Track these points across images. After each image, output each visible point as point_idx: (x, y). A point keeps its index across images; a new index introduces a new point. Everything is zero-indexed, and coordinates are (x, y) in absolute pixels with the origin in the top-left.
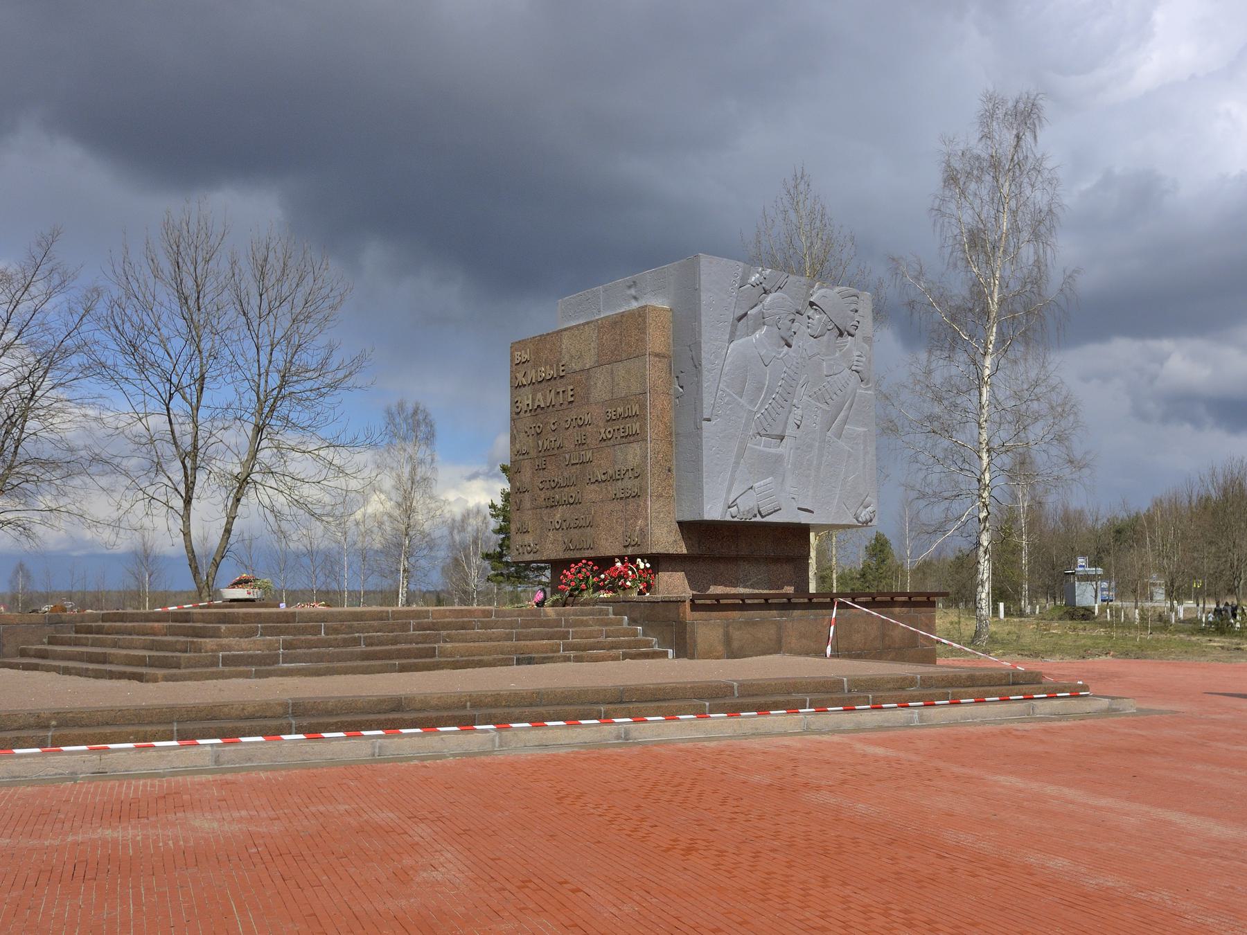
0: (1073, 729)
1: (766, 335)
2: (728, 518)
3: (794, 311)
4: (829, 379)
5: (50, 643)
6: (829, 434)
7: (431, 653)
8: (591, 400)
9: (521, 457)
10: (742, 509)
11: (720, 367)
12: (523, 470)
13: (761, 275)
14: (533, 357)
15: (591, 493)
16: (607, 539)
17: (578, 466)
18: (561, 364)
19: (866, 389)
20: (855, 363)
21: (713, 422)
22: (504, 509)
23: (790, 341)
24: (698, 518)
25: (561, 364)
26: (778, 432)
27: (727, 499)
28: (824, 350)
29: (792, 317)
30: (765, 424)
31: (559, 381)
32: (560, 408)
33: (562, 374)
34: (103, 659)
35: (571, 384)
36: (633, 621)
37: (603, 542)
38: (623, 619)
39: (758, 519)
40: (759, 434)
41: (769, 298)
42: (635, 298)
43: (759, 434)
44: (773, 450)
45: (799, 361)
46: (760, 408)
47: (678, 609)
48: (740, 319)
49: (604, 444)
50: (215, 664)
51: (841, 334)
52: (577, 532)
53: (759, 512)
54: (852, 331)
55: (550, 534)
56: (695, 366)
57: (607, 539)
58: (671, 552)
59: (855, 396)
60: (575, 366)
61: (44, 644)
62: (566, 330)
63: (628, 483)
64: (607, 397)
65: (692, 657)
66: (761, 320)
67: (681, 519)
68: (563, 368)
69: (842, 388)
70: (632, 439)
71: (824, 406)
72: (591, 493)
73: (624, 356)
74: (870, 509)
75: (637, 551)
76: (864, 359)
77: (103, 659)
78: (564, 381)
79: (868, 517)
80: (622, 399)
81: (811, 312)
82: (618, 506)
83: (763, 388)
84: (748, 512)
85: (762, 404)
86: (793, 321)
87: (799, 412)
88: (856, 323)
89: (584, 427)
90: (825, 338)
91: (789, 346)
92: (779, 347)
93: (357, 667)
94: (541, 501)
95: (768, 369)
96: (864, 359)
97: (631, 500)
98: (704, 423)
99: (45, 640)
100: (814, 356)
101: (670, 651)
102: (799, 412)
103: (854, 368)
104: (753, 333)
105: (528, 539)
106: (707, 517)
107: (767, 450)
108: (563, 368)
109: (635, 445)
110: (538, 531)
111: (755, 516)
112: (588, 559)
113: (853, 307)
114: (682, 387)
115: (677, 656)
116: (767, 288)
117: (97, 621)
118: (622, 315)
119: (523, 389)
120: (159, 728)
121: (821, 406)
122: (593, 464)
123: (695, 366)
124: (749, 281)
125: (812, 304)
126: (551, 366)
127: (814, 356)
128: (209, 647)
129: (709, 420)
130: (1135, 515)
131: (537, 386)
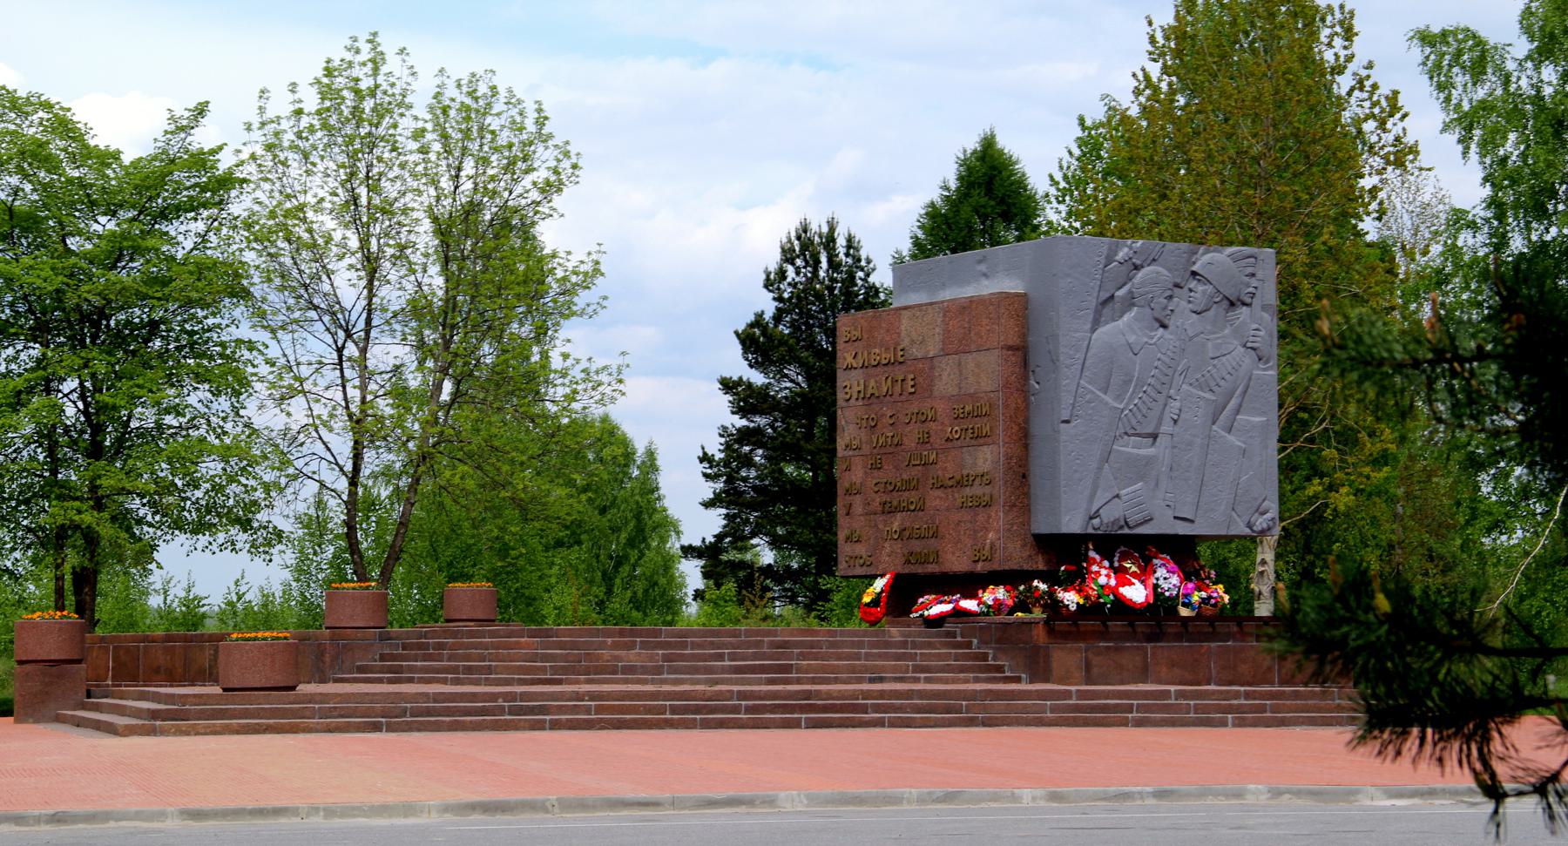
1: (1136, 318)
2: (1090, 531)
3: (1170, 286)
4: (1216, 362)
6: (1215, 427)
7: (786, 669)
8: (936, 393)
9: (851, 453)
10: (1105, 521)
11: (1081, 361)
12: (853, 468)
13: (1131, 248)
14: (865, 336)
15: (935, 499)
16: (953, 553)
18: (900, 348)
19: (1265, 370)
20: (1251, 339)
21: (1072, 424)
22: (726, 463)
23: (1166, 322)
24: (1055, 531)
25: (900, 348)
26: (1149, 430)
27: (1088, 509)
28: (1209, 328)
29: (1168, 293)
30: (1134, 422)
31: (898, 367)
32: (898, 399)
33: (901, 360)
34: (489, 670)
35: (909, 372)
36: (983, 642)
37: (950, 556)
38: (971, 642)
39: (1126, 531)
40: (1126, 433)
41: (1140, 274)
43: (1126, 433)
44: (1143, 452)
45: (1177, 344)
46: (1128, 404)
47: (1031, 630)
48: (1105, 303)
49: (950, 445)
50: (615, 673)
51: (1232, 304)
53: (1126, 523)
54: (1248, 300)
55: (887, 545)
57: (953, 553)
58: (1026, 567)
59: (1250, 379)
60: (916, 352)
62: (906, 308)
63: (977, 490)
64: (953, 391)
66: (1130, 301)
69: (1233, 372)
70: (981, 441)
71: (1208, 395)
72: (935, 499)
73: (973, 347)
74: (1268, 516)
76: (1261, 333)
78: (903, 368)
79: (1265, 526)
80: (971, 395)
81: (1193, 284)
82: (965, 515)
83: (1131, 381)
84: (1113, 523)
85: (1131, 399)
86: (1170, 297)
87: (1177, 404)
88: (1251, 290)
89: (927, 424)
90: (1211, 313)
91: (1164, 326)
92: (1152, 331)
94: (876, 505)
95: (1138, 359)
96: (1261, 333)
97: (981, 509)
98: (1064, 425)
99: (377, 657)
100: (1197, 335)
101: (1024, 676)
102: (1177, 404)
103: (1249, 345)
104: (1121, 316)
105: (861, 550)
106: (1065, 530)
107: (1136, 451)
109: (985, 448)
110: (872, 541)
111: (1121, 527)
113: (1250, 270)
116: (1138, 262)
118: (971, 300)
119: (854, 373)
121: (1203, 394)
122: (938, 467)
124: (1117, 258)
125: (1194, 274)
126: (887, 349)
127: (1197, 335)
128: (605, 658)
129: (1067, 422)
131: (871, 371)
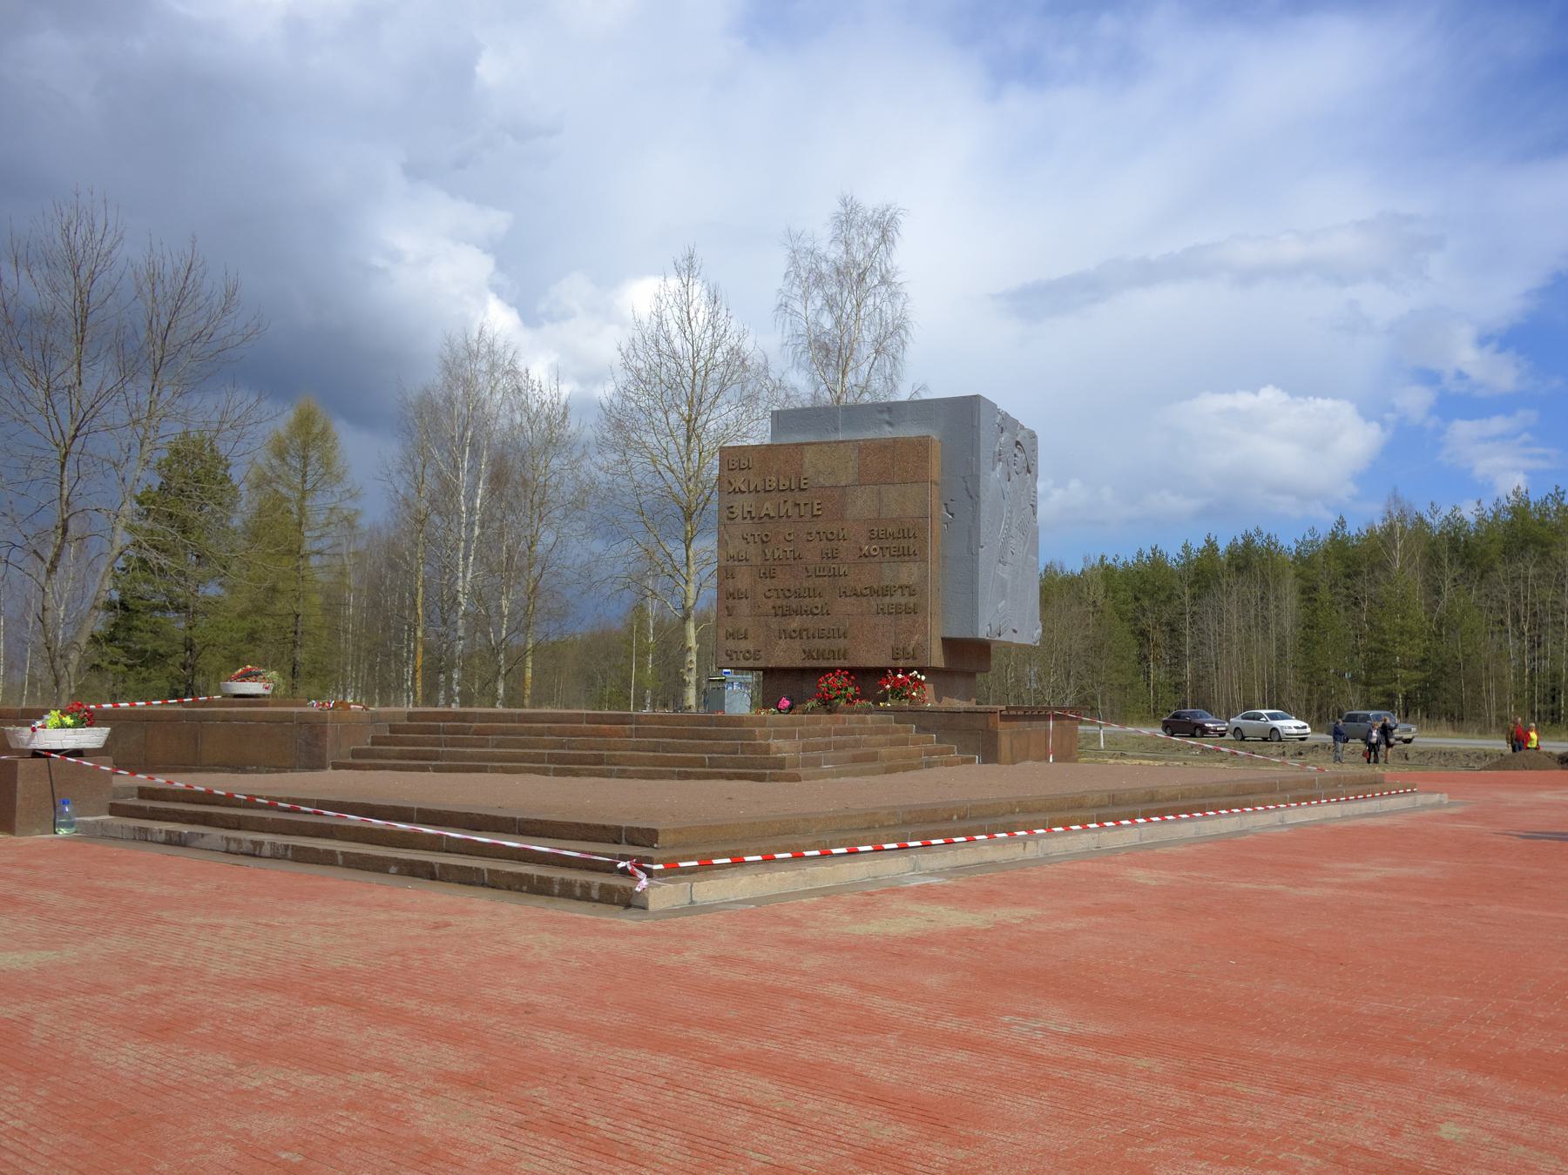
0: (177, 970)
5: (373, 744)
17: (825, 578)
24: (969, 636)
33: (803, 486)
34: (437, 756)
42: (890, 424)
52: (824, 642)
56: (971, 497)
61: (367, 744)
65: (1000, 764)
67: (947, 636)
68: (805, 481)
75: (911, 663)
77: (437, 756)
93: (395, 765)
99: (369, 741)
108: (805, 481)
109: (911, 565)
112: (843, 669)
114: (952, 514)
115: (984, 762)
117: (403, 721)
120: (161, 827)
123: (971, 497)
130: (761, 361)
